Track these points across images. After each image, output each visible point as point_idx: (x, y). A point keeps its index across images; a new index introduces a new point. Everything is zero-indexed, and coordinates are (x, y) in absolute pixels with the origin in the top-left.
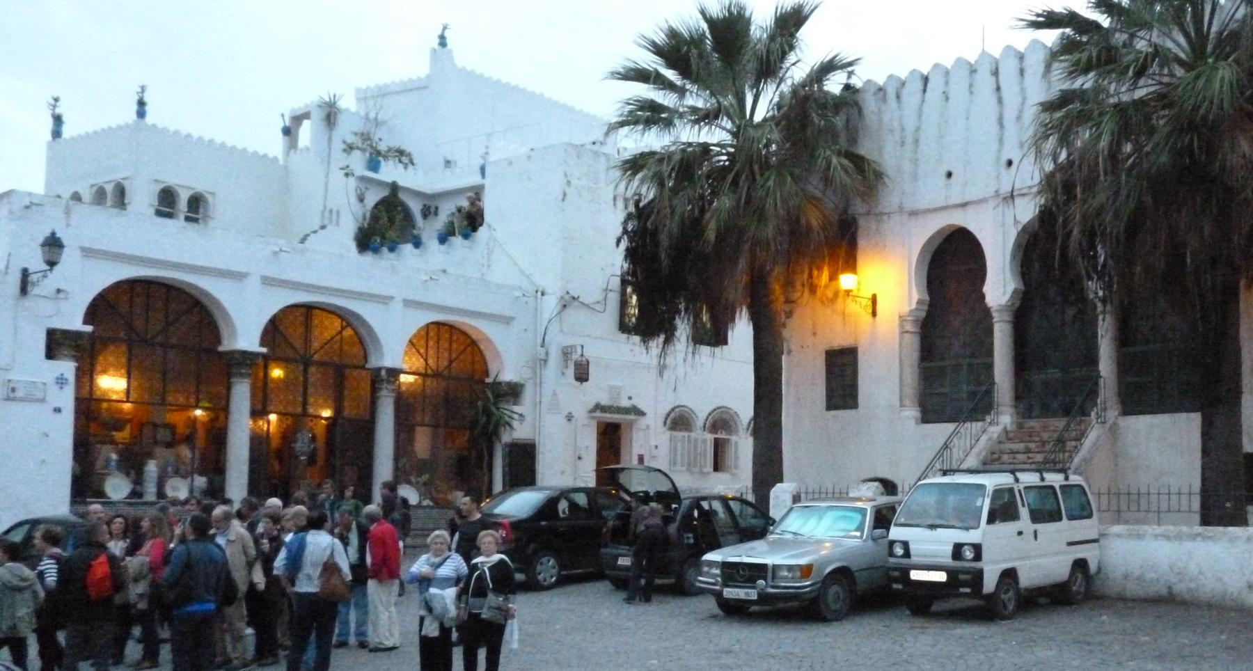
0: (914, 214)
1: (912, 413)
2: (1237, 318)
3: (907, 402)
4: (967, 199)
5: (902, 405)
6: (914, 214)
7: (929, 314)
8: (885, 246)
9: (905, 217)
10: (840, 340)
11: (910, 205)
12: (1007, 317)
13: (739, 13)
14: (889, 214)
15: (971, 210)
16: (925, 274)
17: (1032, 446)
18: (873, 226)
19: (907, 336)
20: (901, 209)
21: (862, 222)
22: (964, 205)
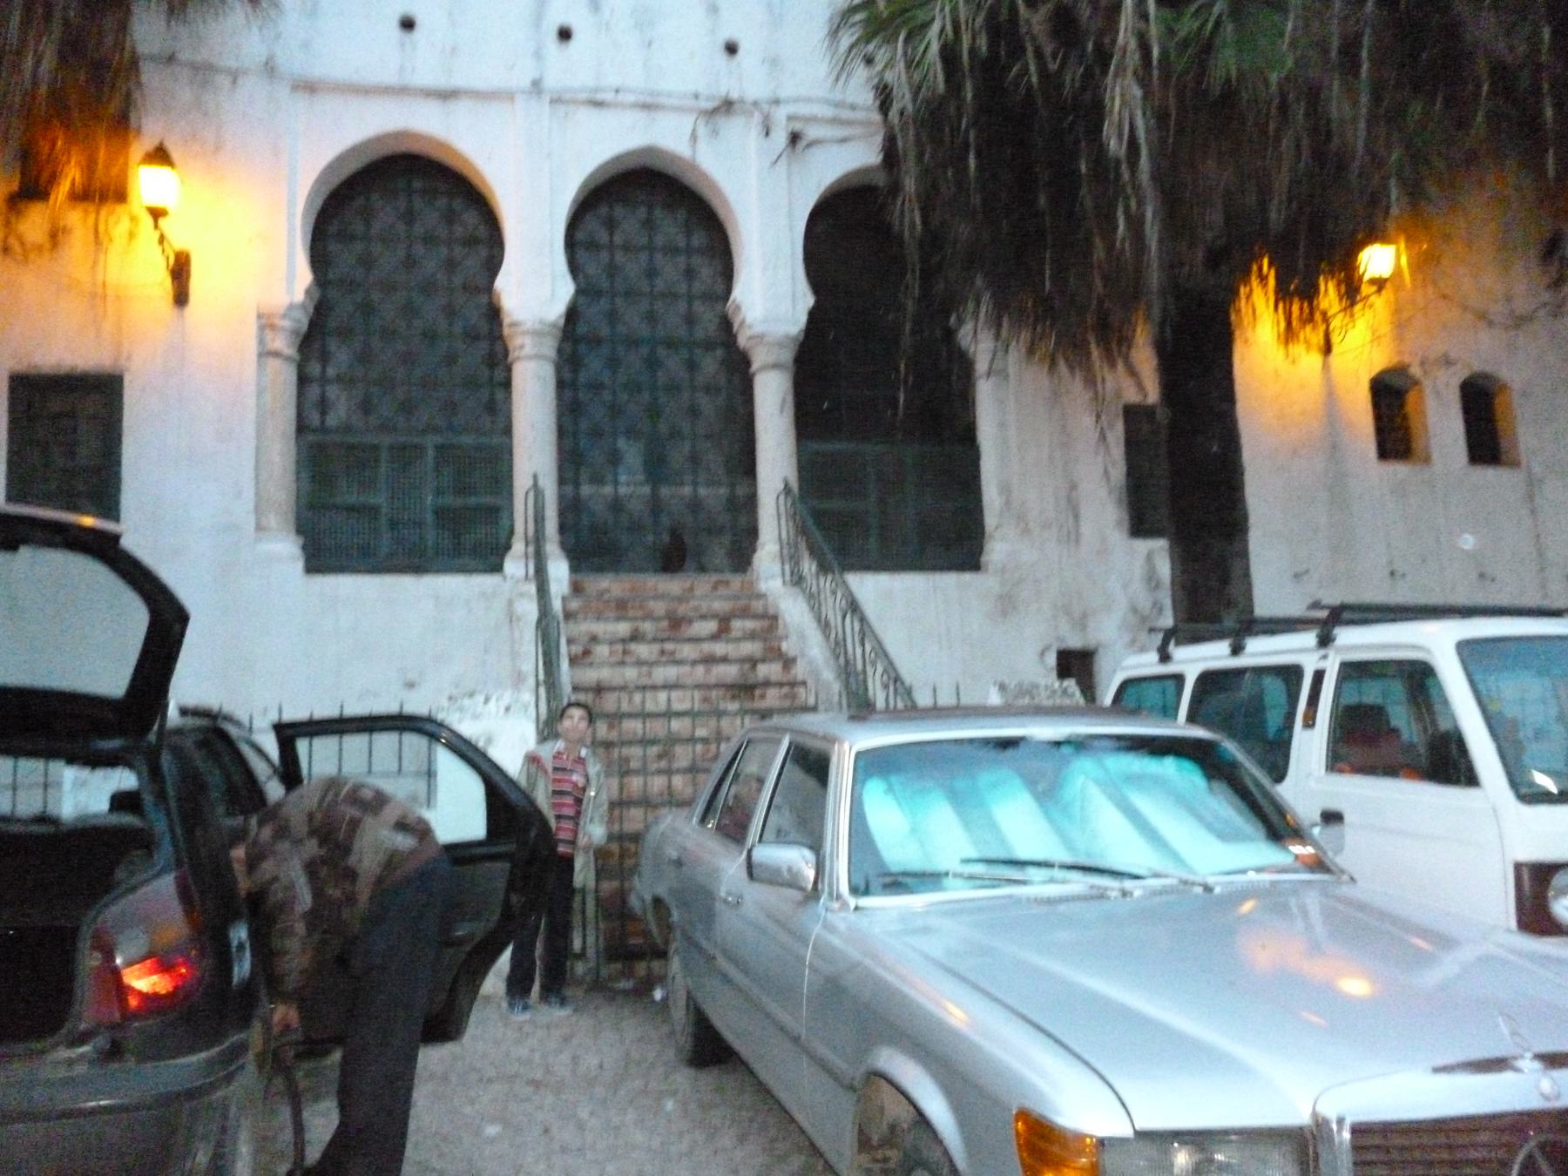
0: (309, 87)
1: (286, 549)
2: (905, 996)
3: (272, 520)
4: (458, 81)
5: (259, 528)
6: (309, 87)
7: (313, 324)
8: (218, 148)
9: (283, 91)
10: (65, 348)
11: (293, 61)
12: (549, 347)
13: (1309, 293)
14: (235, 76)
15: (461, 107)
16: (312, 221)
17: (647, 627)
18: (185, 94)
19: (274, 364)
20: (270, 69)
21: (150, 75)
22: (447, 95)
